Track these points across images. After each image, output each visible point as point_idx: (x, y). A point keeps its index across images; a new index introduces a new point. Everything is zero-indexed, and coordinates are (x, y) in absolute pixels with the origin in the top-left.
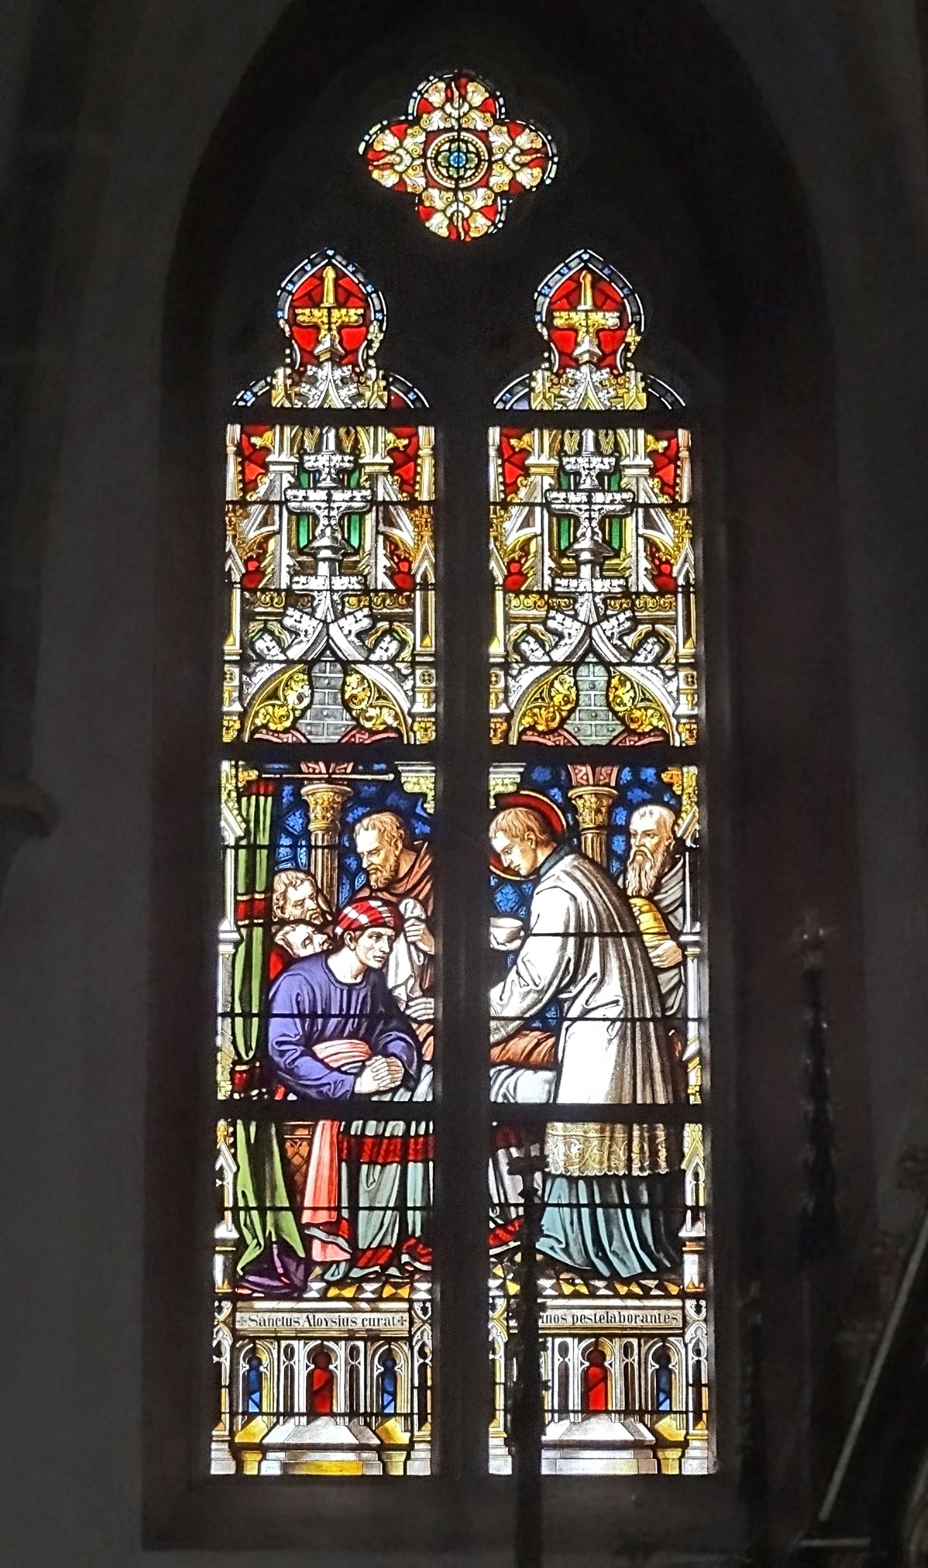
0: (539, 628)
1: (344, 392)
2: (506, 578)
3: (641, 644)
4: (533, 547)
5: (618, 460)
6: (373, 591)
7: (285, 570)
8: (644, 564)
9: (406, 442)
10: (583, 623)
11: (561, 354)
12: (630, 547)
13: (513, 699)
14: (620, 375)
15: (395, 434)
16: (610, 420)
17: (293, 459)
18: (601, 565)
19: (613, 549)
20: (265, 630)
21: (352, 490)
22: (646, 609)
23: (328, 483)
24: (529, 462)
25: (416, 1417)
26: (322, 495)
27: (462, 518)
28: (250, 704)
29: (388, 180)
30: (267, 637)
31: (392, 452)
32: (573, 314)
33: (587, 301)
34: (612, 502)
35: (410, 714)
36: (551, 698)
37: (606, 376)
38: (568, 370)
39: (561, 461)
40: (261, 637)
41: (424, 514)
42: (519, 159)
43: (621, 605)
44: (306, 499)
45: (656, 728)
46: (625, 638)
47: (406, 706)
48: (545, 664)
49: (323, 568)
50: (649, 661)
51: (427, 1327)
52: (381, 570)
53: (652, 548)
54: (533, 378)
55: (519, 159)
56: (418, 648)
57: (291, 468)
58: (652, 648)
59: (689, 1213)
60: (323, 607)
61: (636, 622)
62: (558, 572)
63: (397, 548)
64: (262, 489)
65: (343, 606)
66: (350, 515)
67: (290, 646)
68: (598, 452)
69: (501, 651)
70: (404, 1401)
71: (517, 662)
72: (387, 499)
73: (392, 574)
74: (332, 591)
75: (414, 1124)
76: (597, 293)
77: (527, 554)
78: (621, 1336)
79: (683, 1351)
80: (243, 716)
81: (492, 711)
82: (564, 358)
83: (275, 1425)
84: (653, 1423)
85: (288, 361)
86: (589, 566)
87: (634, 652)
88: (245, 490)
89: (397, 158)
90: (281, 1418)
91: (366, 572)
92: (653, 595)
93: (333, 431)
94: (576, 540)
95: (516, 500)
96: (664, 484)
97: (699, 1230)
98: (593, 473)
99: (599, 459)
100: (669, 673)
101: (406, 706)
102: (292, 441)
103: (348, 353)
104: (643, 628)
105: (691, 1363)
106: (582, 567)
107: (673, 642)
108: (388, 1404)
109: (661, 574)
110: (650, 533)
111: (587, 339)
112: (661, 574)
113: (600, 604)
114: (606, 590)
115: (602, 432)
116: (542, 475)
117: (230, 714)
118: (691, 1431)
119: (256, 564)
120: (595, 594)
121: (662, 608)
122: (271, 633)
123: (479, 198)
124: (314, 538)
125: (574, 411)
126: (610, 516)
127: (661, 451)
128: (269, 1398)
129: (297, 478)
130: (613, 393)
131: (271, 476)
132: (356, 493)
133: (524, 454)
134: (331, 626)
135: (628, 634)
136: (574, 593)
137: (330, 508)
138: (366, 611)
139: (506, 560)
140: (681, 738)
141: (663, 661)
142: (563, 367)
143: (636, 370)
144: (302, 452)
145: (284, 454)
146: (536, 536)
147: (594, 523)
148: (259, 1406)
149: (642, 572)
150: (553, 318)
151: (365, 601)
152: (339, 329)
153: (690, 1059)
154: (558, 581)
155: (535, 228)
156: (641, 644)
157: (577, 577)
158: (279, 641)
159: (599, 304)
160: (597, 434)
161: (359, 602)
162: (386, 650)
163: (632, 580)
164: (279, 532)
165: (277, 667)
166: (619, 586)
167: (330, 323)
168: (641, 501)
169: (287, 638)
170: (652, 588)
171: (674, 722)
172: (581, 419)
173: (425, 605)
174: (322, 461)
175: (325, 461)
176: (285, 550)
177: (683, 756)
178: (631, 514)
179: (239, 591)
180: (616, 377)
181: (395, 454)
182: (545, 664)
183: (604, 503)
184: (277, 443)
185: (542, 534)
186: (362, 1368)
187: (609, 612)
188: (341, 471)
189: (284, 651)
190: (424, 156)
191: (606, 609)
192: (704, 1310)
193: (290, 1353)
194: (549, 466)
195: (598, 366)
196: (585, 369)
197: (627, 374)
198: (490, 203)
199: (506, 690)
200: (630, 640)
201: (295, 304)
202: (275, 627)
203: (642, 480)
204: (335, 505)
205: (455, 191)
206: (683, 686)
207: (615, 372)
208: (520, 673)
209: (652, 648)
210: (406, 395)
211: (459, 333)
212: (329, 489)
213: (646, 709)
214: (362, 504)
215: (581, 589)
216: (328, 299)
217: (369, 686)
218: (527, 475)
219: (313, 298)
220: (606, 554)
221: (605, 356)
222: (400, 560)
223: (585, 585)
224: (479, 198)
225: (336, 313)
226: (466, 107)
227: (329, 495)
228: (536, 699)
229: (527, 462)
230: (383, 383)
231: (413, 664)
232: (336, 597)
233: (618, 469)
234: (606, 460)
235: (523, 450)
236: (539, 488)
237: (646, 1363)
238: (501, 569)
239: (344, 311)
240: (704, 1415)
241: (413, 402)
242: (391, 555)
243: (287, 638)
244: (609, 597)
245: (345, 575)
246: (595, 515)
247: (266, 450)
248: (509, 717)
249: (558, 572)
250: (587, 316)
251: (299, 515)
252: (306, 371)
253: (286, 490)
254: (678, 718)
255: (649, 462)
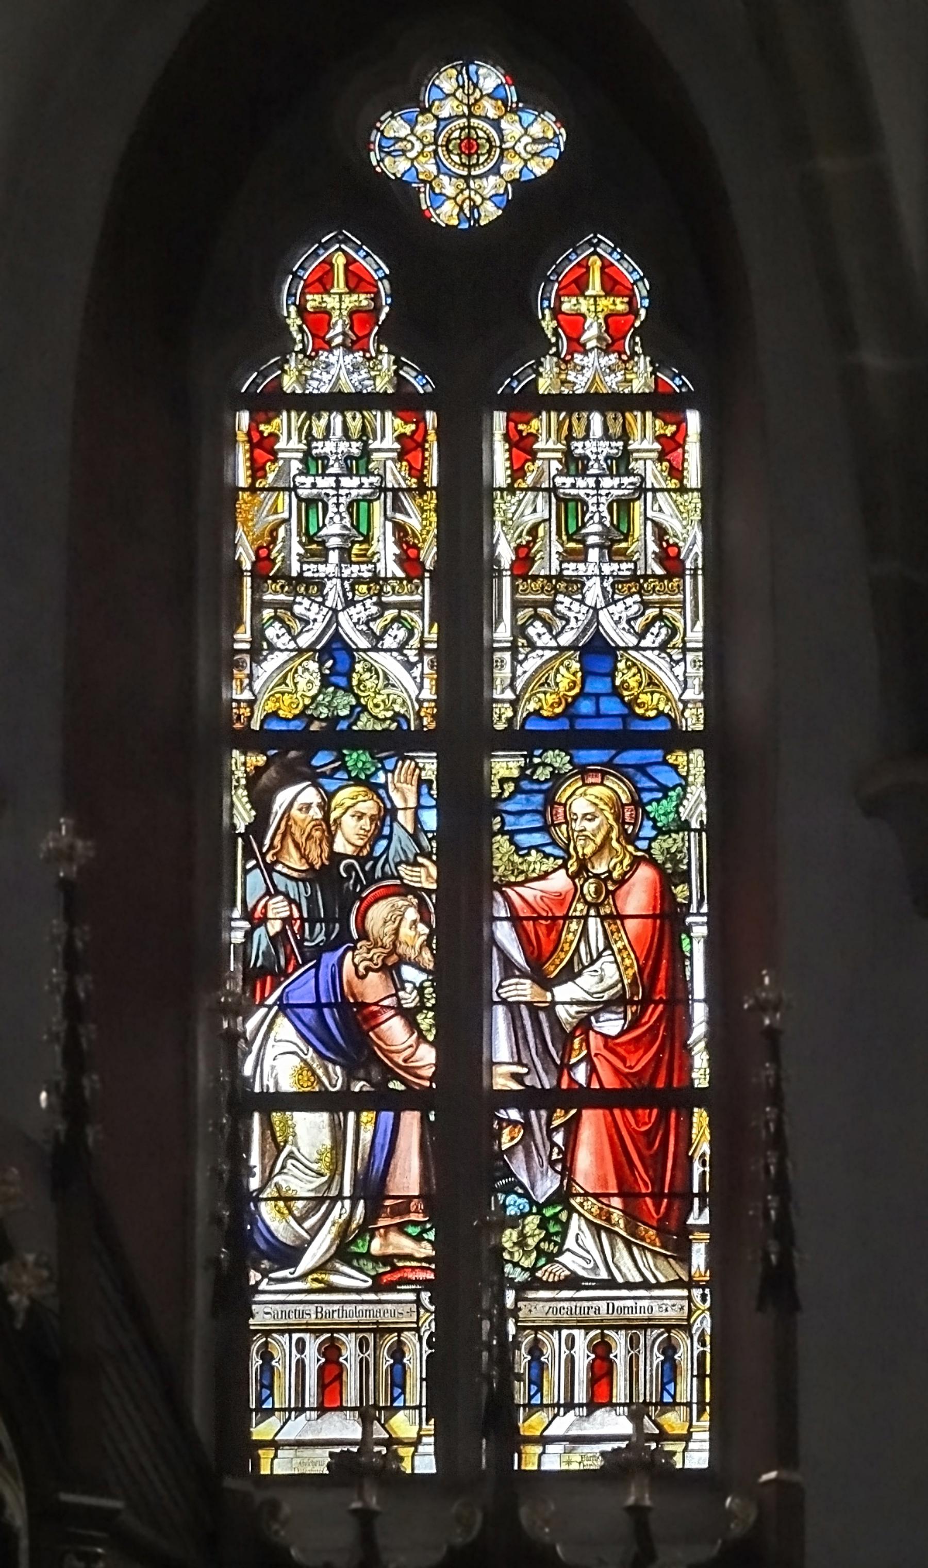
0: (545, 611)
1: (355, 377)
2: (254, 564)
3: (385, 630)
4: (541, 532)
5: (626, 445)
6: (641, 576)
7: (554, 556)
8: (652, 547)
9: (674, 428)
10: (331, 609)
11: (313, 336)
12: (377, 532)
13: (257, 686)
14: (371, 358)
15: (402, 419)
16: (616, 403)
17: (559, 446)
18: (609, 548)
19: (622, 533)
20: (276, 618)
21: (360, 476)
22: (542, 592)
23: (335, 469)
24: (536, 446)
25: (695, 1407)
26: (331, 481)
27: (464, 503)
28: (524, 689)
29: (397, 167)
30: (277, 625)
31: (400, 438)
32: (326, 298)
33: (340, 284)
34: (620, 486)
35: (418, 700)
36: (557, 684)
37: (614, 361)
38: (576, 355)
39: (568, 446)
40: (531, 624)
41: (431, 500)
42: (532, 142)
43: (630, 588)
44: (314, 486)
45: (660, 714)
46: (371, 624)
47: (675, 690)
48: (551, 649)
49: (334, 557)
50: (656, 645)
51: (707, 1314)
52: (391, 558)
53: (400, 529)
54: (541, 364)
55: (532, 142)
56: (426, 635)
57: (559, 455)
58: (659, 633)
59: (696, 1201)
60: (333, 595)
61: (384, 607)
62: (568, 556)
63: (406, 534)
64: (271, 476)
65: (354, 595)
66: (358, 501)
67: (301, 633)
68: (607, 436)
69: (247, 636)
70: (686, 1388)
71: (523, 646)
72: (396, 486)
73: (401, 561)
74: (343, 580)
75: (533, 1113)
76: (605, 277)
77: (535, 538)
78: (357, 1331)
79: (689, 1342)
80: (514, 704)
81: (495, 696)
82: (317, 340)
83: (287, 1421)
84: (386, 1421)
85: (554, 350)
86: (597, 550)
87: (641, 636)
88: (254, 477)
89: (404, 146)
90: (562, 1410)
91: (374, 560)
92: (661, 578)
93: (339, 418)
94: (584, 525)
95: (524, 485)
96: (411, 468)
97: (705, 1219)
98: (601, 457)
99: (607, 443)
100: (676, 657)
101: (414, 691)
102: (300, 429)
103: (614, 341)
104: (390, 614)
105: (563, 1357)
106: (591, 550)
107: (680, 625)
108: (267, 1398)
109: (668, 557)
110: (400, 517)
111: (340, 322)
112: (409, 560)
113: (609, 589)
114: (354, 575)
115: (611, 415)
116: (549, 459)
117: (502, 701)
118: (695, 1423)
119: (526, 550)
120: (343, 580)
121: (672, 592)
122: (282, 621)
123: (491, 185)
124: (324, 525)
125: (582, 395)
126: (619, 500)
127: (408, 433)
128: (553, 1389)
129: (566, 465)
130: (365, 376)
131: (281, 462)
132: (364, 480)
133: (272, 439)
134: (600, 612)
135: (374, 620)
136: (581, 576)
137: (338, 496)
138: (375, 599)
139: (513, 545)
140: (694, 721)
141: (671, 645)
142: (571, 352)
143: (389, 353)
144: (570, 438)
145: (551, 441)
146: (544, 521)
147: (342, 508)
148: (674, 1397)
149: (650, 556)
150: (561, 303)
151: (375, 588)
152: (606, 318)
153: (696, 1043)
154: (305, 567)
155: (542, 217)
156: (385, 630)
157: (585, 561)
158: (289, 630)
159: (352, 286)
160: (344, 417)
161: (369, 589)
162: (395, 637)
163: (641, 564)
164: (287, 521)
165: (548, 654)
166: (369, 571)
167: (340, 309)
168: (389, 485)
169: (297, 626)
170: (659, 571)
171: (681, 706)
172: (338, 401)
173: (693, 590)
174: (329, 447)
175: (596, 450)
176: (295, 539)
177: (687, 741)
178: (639, 498)
179: (509, 579)
180: (624, 362)
181: (662, 440)
182: (551, 649)
183: (612, 488)
184: (286, 430)
185: (549, 520)
186: (642, 1357)
187: (616, 597)
188: (350, 457)
189: (294, 638)
190: (435, 142)
191: (614, 593)
192: (708, 1298)
193: (301, 1346)
194: (297, 450)
195: (607, 351)
196: (592, 355)
197: (380, 357)
198: (501, 191)
199: (250, 676)
200: (377, 627)
201: (561, 293)
202: (287, 616)
203: (649, 462)
204: (603, 492)
205: (466, 179)
206: (427, 670)
207: (368, 355)
208: (526, 658)
209: (659, 633)
210: (673, 380)
211: (465, 317)
212: (337, 475)
213: (652, 693)
214: (370, 491)
215: (589, 573)
216: (337, 286)
217: (639, 671)
218: (275, 460)
219: (323, 283)
220: (359, 536)
221: (359, 339)
222: (409, 547)
223: (592, 569)
224: (491, 185)
225: (346, 299)
226: (477, 94)
227: (338, 482)
228: (542, 685)
229: (277, 447)
230: (556, 370)
231: (422, 651)
232: (347, 584)
233: (366, 453)
234: (614, 444)
235: (530, 434)
236: (546, 474)
237: (652, 1351)
238: (248, 555)
239: (355, 297)
240: (708, 1408)
241: (679, 387)
242: (399, 542)
243: (297, 626)
244: (618, 580)
245: (615, 562)
246: (603, 499)
247: (535, 437)
248: (251, 704)
249: (568, 556)
250: (595, 301)
251: (566, 501)
252: (572, 358)
253: (295, 477)
254: (685, 703)
255: (657, 446)
